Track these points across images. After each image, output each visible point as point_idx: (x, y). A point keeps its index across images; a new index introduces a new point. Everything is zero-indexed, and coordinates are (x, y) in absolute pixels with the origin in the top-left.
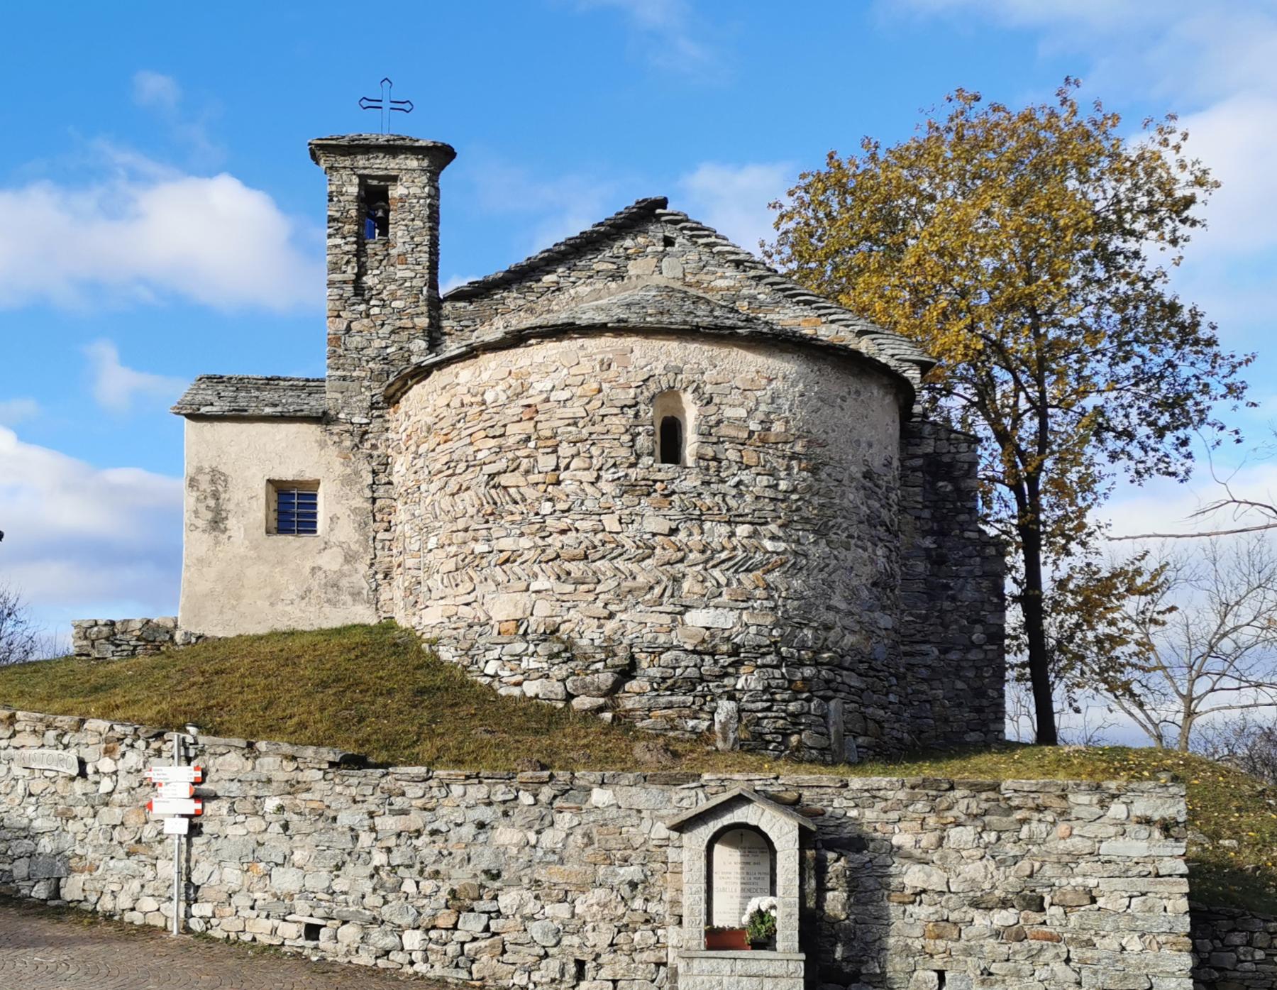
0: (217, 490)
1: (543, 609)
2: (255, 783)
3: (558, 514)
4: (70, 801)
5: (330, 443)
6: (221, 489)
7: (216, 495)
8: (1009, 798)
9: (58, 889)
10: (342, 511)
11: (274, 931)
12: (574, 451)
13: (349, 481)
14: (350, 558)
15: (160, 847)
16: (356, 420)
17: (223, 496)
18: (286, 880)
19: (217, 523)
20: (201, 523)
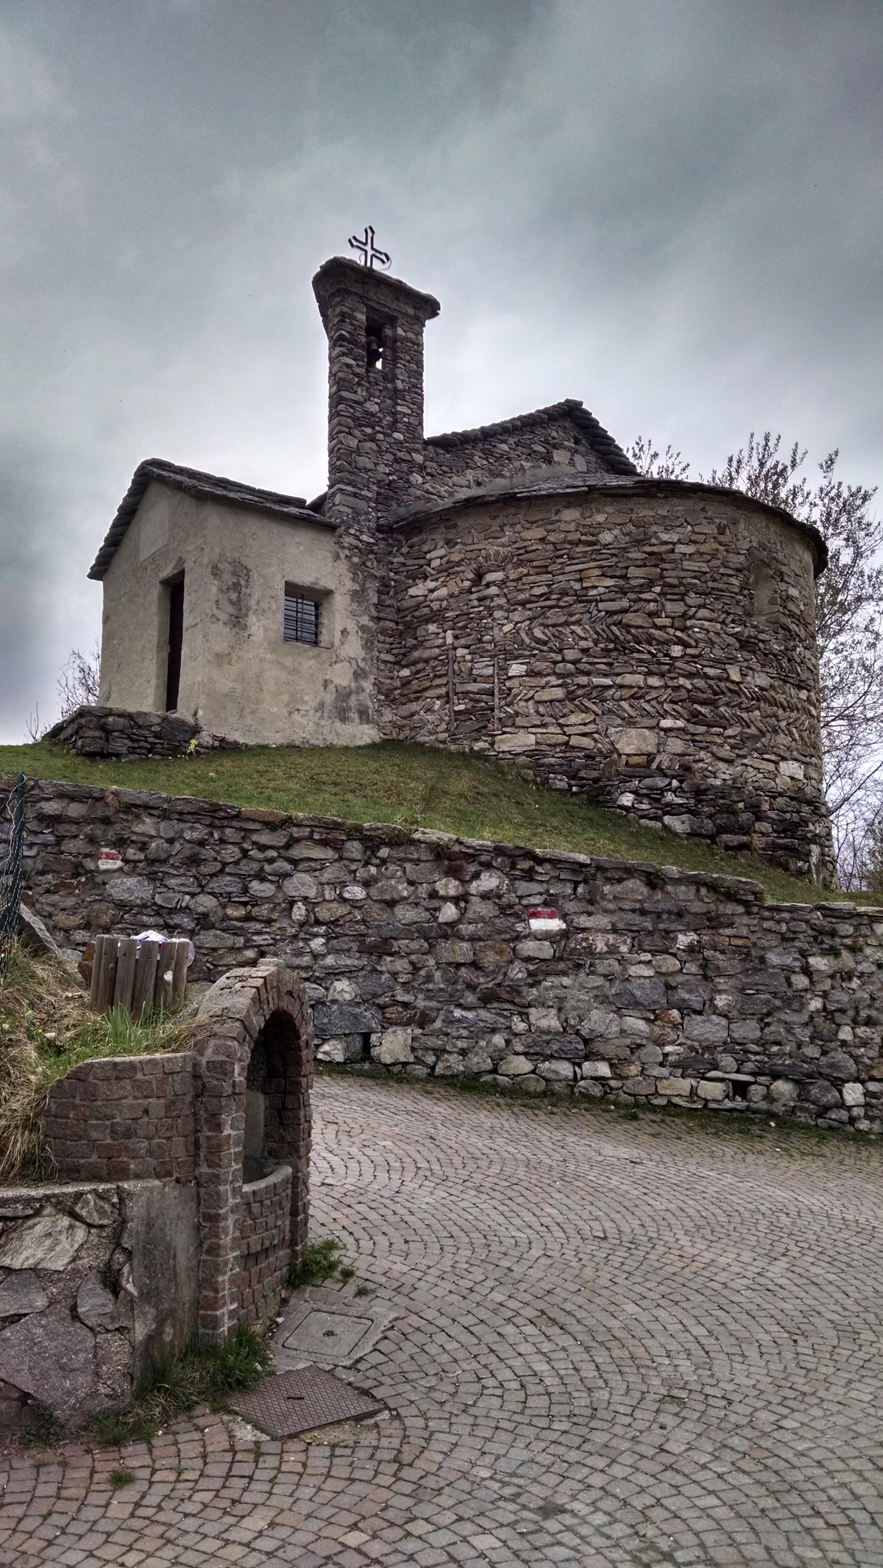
0: (239, 584)
1: (676, 745)
2: (665, 916)
3: (688, 658)
4: (386, 932)
5: (342, 556)
6: (243, 583)
7: (236, 586)
8: (273, 910)
9: (367, 1046)
10: (351, 626)
11: (693, 1092)
12: (700, 601)
13: (358, 596)
14: (359, 674)
15: (534, 991)
16: (365, 538)
17: (244, 590)
18: (708, 1029)
19: (238, 621)
20: (223, 617)
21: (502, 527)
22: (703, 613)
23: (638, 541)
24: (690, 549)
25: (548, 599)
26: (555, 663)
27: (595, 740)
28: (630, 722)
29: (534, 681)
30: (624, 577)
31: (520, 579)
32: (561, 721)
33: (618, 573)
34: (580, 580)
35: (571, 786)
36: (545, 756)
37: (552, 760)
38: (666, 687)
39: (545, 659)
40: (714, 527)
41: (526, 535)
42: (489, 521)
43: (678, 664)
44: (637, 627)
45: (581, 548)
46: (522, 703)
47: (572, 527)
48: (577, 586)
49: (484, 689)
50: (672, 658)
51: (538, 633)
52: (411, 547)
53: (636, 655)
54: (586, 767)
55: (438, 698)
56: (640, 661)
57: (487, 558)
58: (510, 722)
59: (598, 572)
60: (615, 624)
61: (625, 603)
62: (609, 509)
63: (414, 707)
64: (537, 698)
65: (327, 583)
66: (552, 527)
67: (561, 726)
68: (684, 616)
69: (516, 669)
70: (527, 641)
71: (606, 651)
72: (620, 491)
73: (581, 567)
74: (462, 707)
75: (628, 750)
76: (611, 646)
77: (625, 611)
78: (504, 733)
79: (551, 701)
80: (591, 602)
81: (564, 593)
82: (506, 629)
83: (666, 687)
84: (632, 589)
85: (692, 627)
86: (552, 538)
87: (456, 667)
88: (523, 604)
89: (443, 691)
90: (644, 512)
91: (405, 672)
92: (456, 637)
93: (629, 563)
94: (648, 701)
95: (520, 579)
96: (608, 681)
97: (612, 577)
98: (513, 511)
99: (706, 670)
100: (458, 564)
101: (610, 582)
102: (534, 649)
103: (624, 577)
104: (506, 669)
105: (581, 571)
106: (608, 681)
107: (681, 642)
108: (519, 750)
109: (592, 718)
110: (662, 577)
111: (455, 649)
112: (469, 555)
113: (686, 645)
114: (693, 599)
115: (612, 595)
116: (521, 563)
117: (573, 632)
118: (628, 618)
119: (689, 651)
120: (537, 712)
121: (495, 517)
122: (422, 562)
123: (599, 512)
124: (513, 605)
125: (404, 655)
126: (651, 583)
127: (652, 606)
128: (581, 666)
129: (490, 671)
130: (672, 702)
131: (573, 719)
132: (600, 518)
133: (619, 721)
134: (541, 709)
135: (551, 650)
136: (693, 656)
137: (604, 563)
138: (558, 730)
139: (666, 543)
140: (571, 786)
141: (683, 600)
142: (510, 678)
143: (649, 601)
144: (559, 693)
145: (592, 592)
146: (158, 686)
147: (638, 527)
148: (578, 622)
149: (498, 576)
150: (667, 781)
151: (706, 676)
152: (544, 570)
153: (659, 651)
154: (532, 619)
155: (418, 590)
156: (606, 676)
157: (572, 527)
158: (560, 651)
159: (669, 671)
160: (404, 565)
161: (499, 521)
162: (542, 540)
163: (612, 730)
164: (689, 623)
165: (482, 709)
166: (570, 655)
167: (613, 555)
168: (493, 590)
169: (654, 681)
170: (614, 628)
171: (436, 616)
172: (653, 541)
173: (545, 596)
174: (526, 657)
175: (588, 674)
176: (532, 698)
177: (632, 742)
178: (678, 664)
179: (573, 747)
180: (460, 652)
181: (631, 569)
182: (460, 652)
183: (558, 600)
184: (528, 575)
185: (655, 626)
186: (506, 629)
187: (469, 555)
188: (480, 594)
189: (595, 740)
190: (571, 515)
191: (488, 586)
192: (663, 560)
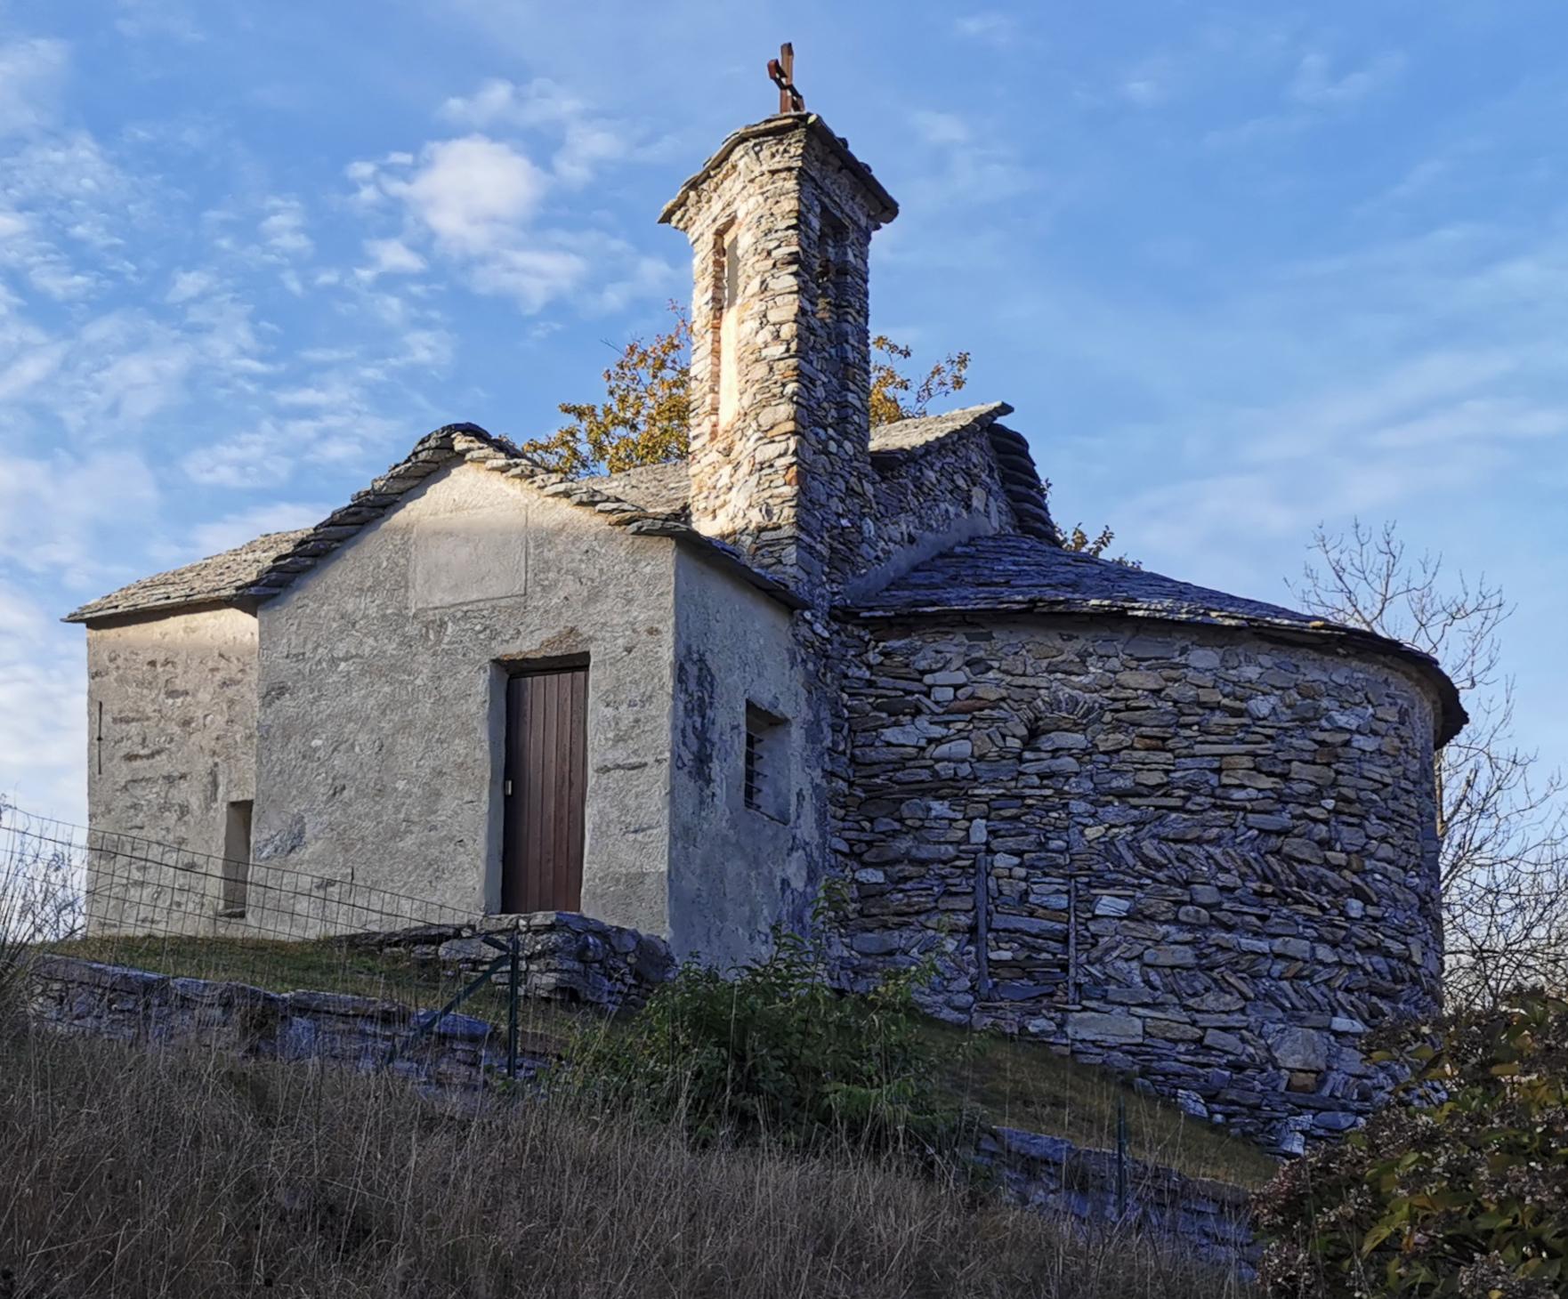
21: (1083, 657)
22: (1385, 851)
23: (1304, 720)
24: (1369, 744)
25: (1165, 795)
26: (1179, 903)
27: (1243, 1040)
28: (1293, 1016)
29: (1144, 930)
30: (1285, 777)
31: (1117, 751)
32: (1191, 1002)
33: (1278, 770)
34: (1218, 771)
35: (1211, 1113)
36: (1160, 1058)
37: (1176, 1066)
38: (1340, 964)
39: (1163, 895)
40: (1395, 710)
41: (1125, 677)
42: (1059, 643)
43: (1355, 929)
44: (1301, 861)
45: (1218, 718)
46: (1120, 964)
47: (1207, 679)
48: (1214, 781)
49: (1052, 931)
50: (1348, 918)
51: (1149, 848)
52: (886, 654)
53: (1302, 908)
54: (1231, 1083)
55: (953, 931)
56: (1310, 918)
57: (1054, 705)
58: (1096, 992)
59: (1247, 762)
60: (1271, 853)
61: (1285, 819)
62: (1266, 660)
63: (896, 939)
64: (1147, 958)
65: (785, 708)
66: (1174, 674)
67: (1186, 1008)
68: (1363, 852)
69: (1109, 904)
70: (1128, 856)
71: (1260, 894)
72: (1300, 638)
73: (1221, 749)
74: (1007, 955)
75: (1291, 1063)
76: (1269, 889)
77: (1284, 833)
78: (1085, 1009)
79: (1172, 967)
80: (1237, 809)
81: (1193, 790)
82: (1091, 833)
83: (1340, 964)
84: (1295, 798)
85: (1373, 871)
86: (1173, 690)
87: (992, 884)
88: (1122, 795)
89: (964, 920)
90: (1313, 673)
91: (874, 876)
92: (993, 833)
93: (1292, 755)
94: (1314, 985)
95: (1117, 751)
96: (1263, 946)
97: (1270, 774)
98: (1107, 634)
99: (1389, 943)
100: (995, 705)
101: (1267, 783)
102: (1140, 875)
103: (1285, 777)
104: (1093, 900)
105: (1222, 755)
106: (1263, 946)
107: (1358, 893)
108: (1111, 1040)
109: (1242, 1004)
110: (1334, 784)
111: (990, 851)
112: (1017, 694)
113: (1367, 901)
114: (1374, 826)
115: (1268, 804)
116: (1117, 726)
117: (1210, 857)
118: (1291, 846)
119: (1371, 910)
120: (1147, 982)
121: (1070, 638)
122: (915, 686)
123: (1249, 661)
124: (1100, 797)
125: (870, 844)
126: (1319, 794)
127: (1322, 831)
128: (1224, 916)
129: (1063, 902)
130: (1348, 990)
131: (1210, 1001)
132: (1251, 672)
133: (1280, 1014)
134: (1154, 977)
135: (1172, 881)
136: (1375, 919)
137: (1259, 749)
138: (1183, 1016)
139: (1341, 729)
140: (1211, 1113)
141: (1360, 825)
142: (1095, 917)
143: (1315, 820)
144: (1187, 956)
145: (1238, 795)
146: (489, 856)
147: (1304, 698)
148: (1216, 841)
149: (1077, 740)
150: (1352, 1119)
151: (1388, 954)
152: (1160, 744)
153: (1334, 906)
154: (1138, 824)
155: (905, 735)
156: (1256, 934)
157: (1207, 679)
158: (1186, 884)
159: (1345, 940)
160: (871, 684)
161: (1078, 645)
162: (1156, 693)
163: (1269, 1027)
164: (1368, 864)
165: (1046, 963)
166: (1206, 894)
167: (1269, 737)
168: (1068, 763)
169: (1324, 952)
170: (1269, 857)
171: (955, 789)
172: (1324, 723)
173: (1165, 789)
174: (1125, 885)
175: (1229, 929)
176: (1139, 957)
177: (1296, 1051)
178: (1355, 929)
179: (1209, 1048)
180: (1002, 860)
181: (1295, 764)
182: (1002, 860)
183: (1186, 799)
184: (1131, 747)
185: (1327, 863)
186: (1091, 833)
187: (1017, 694)
188: (1042, 766)
189: (1243, 1040)
190: (1204, 658)
191: (1055, 753)
192: (1338, 757)
